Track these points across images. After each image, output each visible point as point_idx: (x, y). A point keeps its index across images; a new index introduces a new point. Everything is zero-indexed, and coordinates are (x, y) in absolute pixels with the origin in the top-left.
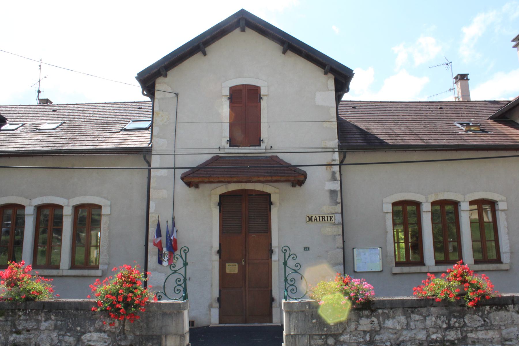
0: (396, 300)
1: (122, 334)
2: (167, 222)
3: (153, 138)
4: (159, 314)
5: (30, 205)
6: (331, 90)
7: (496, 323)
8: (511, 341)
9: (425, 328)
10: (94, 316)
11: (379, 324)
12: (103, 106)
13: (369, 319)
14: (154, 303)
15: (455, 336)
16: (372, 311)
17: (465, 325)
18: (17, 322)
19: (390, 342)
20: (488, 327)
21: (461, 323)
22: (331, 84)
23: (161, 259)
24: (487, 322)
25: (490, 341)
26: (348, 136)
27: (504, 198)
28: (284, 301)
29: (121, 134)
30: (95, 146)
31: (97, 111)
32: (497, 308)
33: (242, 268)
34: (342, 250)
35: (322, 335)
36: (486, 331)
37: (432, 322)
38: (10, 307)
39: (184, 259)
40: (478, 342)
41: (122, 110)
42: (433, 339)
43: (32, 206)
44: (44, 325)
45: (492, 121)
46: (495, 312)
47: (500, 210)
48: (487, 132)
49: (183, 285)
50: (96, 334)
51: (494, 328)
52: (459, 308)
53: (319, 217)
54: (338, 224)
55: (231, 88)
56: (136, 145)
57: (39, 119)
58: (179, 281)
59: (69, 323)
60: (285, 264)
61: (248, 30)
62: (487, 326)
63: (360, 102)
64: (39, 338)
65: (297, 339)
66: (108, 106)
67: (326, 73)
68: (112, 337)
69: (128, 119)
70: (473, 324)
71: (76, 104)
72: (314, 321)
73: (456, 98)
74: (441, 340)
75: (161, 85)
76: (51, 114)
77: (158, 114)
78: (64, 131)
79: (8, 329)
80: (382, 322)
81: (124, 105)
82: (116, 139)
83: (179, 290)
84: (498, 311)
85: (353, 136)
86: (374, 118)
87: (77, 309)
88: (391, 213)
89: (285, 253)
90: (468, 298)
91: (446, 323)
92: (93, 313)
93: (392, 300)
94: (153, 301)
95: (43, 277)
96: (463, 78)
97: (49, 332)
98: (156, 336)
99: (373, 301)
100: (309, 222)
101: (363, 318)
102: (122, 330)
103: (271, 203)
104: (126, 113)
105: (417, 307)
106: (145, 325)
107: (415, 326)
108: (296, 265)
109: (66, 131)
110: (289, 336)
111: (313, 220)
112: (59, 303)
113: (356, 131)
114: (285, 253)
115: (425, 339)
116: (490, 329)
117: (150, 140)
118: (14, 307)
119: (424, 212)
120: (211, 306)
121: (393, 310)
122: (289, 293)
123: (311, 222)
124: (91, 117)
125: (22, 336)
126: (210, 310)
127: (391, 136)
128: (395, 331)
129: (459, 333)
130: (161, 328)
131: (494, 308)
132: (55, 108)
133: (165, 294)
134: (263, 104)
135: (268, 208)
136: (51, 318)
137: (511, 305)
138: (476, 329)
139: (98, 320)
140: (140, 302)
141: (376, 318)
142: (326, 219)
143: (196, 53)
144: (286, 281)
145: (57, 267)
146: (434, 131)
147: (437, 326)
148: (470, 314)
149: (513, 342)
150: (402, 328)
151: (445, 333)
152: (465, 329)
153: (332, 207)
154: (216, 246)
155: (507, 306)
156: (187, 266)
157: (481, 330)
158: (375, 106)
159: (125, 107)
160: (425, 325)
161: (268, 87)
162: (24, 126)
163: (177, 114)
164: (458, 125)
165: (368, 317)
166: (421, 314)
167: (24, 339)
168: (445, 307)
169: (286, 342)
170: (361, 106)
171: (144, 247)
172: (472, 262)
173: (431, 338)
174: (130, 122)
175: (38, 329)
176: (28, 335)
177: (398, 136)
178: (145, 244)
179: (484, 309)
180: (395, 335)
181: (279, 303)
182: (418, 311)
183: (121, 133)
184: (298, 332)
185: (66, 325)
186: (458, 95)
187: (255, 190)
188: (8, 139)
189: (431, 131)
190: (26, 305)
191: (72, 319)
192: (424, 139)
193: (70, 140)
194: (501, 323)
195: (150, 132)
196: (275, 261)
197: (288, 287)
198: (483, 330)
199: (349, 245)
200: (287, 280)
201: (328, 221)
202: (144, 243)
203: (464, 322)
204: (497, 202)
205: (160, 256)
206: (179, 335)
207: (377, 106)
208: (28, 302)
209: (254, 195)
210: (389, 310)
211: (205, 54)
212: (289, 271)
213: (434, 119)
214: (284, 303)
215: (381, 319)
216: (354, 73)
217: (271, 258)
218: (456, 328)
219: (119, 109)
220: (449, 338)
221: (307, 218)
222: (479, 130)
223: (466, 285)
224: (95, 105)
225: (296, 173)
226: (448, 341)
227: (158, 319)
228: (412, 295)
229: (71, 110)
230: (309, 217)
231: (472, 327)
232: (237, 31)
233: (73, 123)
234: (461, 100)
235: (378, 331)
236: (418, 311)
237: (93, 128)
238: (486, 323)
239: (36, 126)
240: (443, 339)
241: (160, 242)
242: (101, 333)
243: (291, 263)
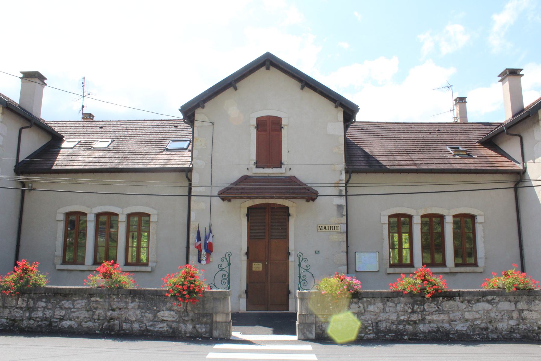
0: (376, 292)
1: (185, 312)
2: (205, 229)
3: (193, 160)
4: (211, 299)
5: (91, 213)
6: (340, 122)
7: (446, 309)
8: (456, 321)
9: (396, 312)
10: (165, 300)
11: (364, 308)
12: (143, 123)
13: (357, 305)
14: (208, 291)
15: (417, 318)
16: (359, 299)
17: (424, 310)
18: (112, 303)
19: (371, 320)
20: (441, 312)
21: (422, 309)
22: (340, 116)
23: (200, 259)
24: (440, 309)
25: (441, 321)
26: (354, 159)
27: (482, 213)
28: (298, 291)
29: (164, 154)
30: (145, 166)
31: (138, 128)
32: (448, 299)
33: (265, 267)
34: (346, 253)
35: (324, 315)
36: (439, 315)
37: (401, 308)
38: (107, 293)
39: (228, 261)
40: (433, 322)
41: (161, 128)
42: (401, 320)
43: (93, 213)
44: (131, 305)
45: (479, 144)
46: (446, 302)
47: (478, 223)
48: (472, 156)
49: (228, 279)
50: (167, 312)
51: (445, 312)
52: (420, 299)
53: (328, 226)
54: (343, 233)
55: (257, 119)
56: (179, 165)
57: (90, 136)
58: (225, 276)
59: (148, 304)
60: (299, 265)
61: (272, 69)
62: (440, 311)
63: (369, 122)
64: (128, 314)
65: (307, 317)
66: (147, 123)
67: (336, 107)
68: (178, 314)
69: (167, 138)
70: (430, 310)
71: (119, 121)
72: (319, 305)
73: (455, 118)
74: (407, 320)
75: (200, 115)
76: (99, 131)
77: (197, 140)
78: (115, 149)
79: (106, 307)
80: (366, 307)
81: (161, 123)
82: (161, 159)
83: (225, 283)
84: (448, 301)
85: (358, 159)
86: (378, 140)
87: (153, 294)
88: (388, 224)
89: (299, 258)
90: (427, 292)
91: (411, 309)
92: (165, 297)
93: (373, 292)
94: (207, 290)
95: (128, 272)
96: (461, 101)
97: (135, 310)
98: (209, 314)
99: (360, 292)
100: (320, 230)
101: (353, 304)
102: (185, 310)
103: (289, 215)
104: (164, 132)
105: (391, 297)
106: (201, 306)
107: (389, 310)
108: (307, 266)
109: (117, 149)
110: (301, 315)
111: (323, 229)
112: (141, 291)
113: (361, 154)
114: (299, 258)
115: (396, 319)
116: (441, 313)
117: (190, 160)
118: (109, 293)
119: (415, 223)
120: (240, 297)
121: (374, 298)
122: (302, 285)
123: (321, 230)
124: (135, 136)
125: (116, 312)
126: (239, 300)
127: (390, 159)
128: (375, 313)
129: (420, 316)
130: (213, 308)
131: (445, 299)
132: (102, 124)
133: (215, 285)
134: (284, 132)
135: (287, 218)
136: (135, 301)
137: (457, 297)
138: (432, 313)
139: (169, 302)
140: (199, 289)
141: (362, 304)
142: (333, 228)
143: (229, 88)
144: (300, 277)
145: (83, 264)
146: (427, 155)
147: (405, 310)
148: (428, 303)
149: (457, 322)
150: (380, 312)
151: (410, 315)
152: (424, 313)
153: (339, 218)
154: (245, 249)
155: (454, 298)
156: (230, 266)
157: (435, 314)
158: (381, 127)
159: (163, 125)
160: (396, 310)
161: (288, 118)
162: (79, 143)
163: (213, 140)
164: (449, 149)
165: (356, 303)
166: (394, 302)
167: (117, 315)
168: (411, 298)
169: (299, 319)
170: (369, 127)
171: (186, 249)
172: (453, 265)
173: (400, 319)
174: (170, 141)
175: (126, 308)
176: (120, 312)
177: (395, 159)
178: (186, 246)
179: (438, 300)
180: (375, 316)
181: (295, 295)
182: (392, 300)
183: (164, 153)
184: (307, 312)
185: (146, 305)
186: (457, 115)
187: (276, 204)
188: (71, 157)
189: (424, 155)
190: (118, 291)
191: (150, 301)
192: (417, 163)
193: (123, 159)
194: (449, 310)
195: (190, 153)
196: (292, 262)
197: (301, 282)
198: (437, 314)
199: (352, 249)
200: (301, 276)
201: (335, 230)
202: (185, 245)
203: (424, 308)
204: (476, 216)
205: (200, 256)
206: (225, 313)
207: (382, 128)
208: (119, 290)
209: (275, 208)
210: (371, 298)
211: (236, 89)
212: (302, 270)
213: (430, 142)
214: (298, 292)
215: (365, 305)
216: (359, 109)
217: (288, 259)
218: (418, 312)
219: (157, 126)
220: (413, 319)
221: (318, 227)
222: (466, 154)
223: (426, 282)
224: (136, 122)
225: (309, 192)
226: (412, 321)
227: (210, 302)
228: (389, 289)
229: (115, 127)
230: (319, 226)
231: (429, 312)
232: (263, 69)
233: (121, 141)
234: (459, 121)
235: (363, 313)
236: (392, 300)
237: (140, 147)
238: (439, 309)
239: (91, 143)
240: (408, 320)
241: (200, 245)
242: (171, 311)
243: (303, 264)
